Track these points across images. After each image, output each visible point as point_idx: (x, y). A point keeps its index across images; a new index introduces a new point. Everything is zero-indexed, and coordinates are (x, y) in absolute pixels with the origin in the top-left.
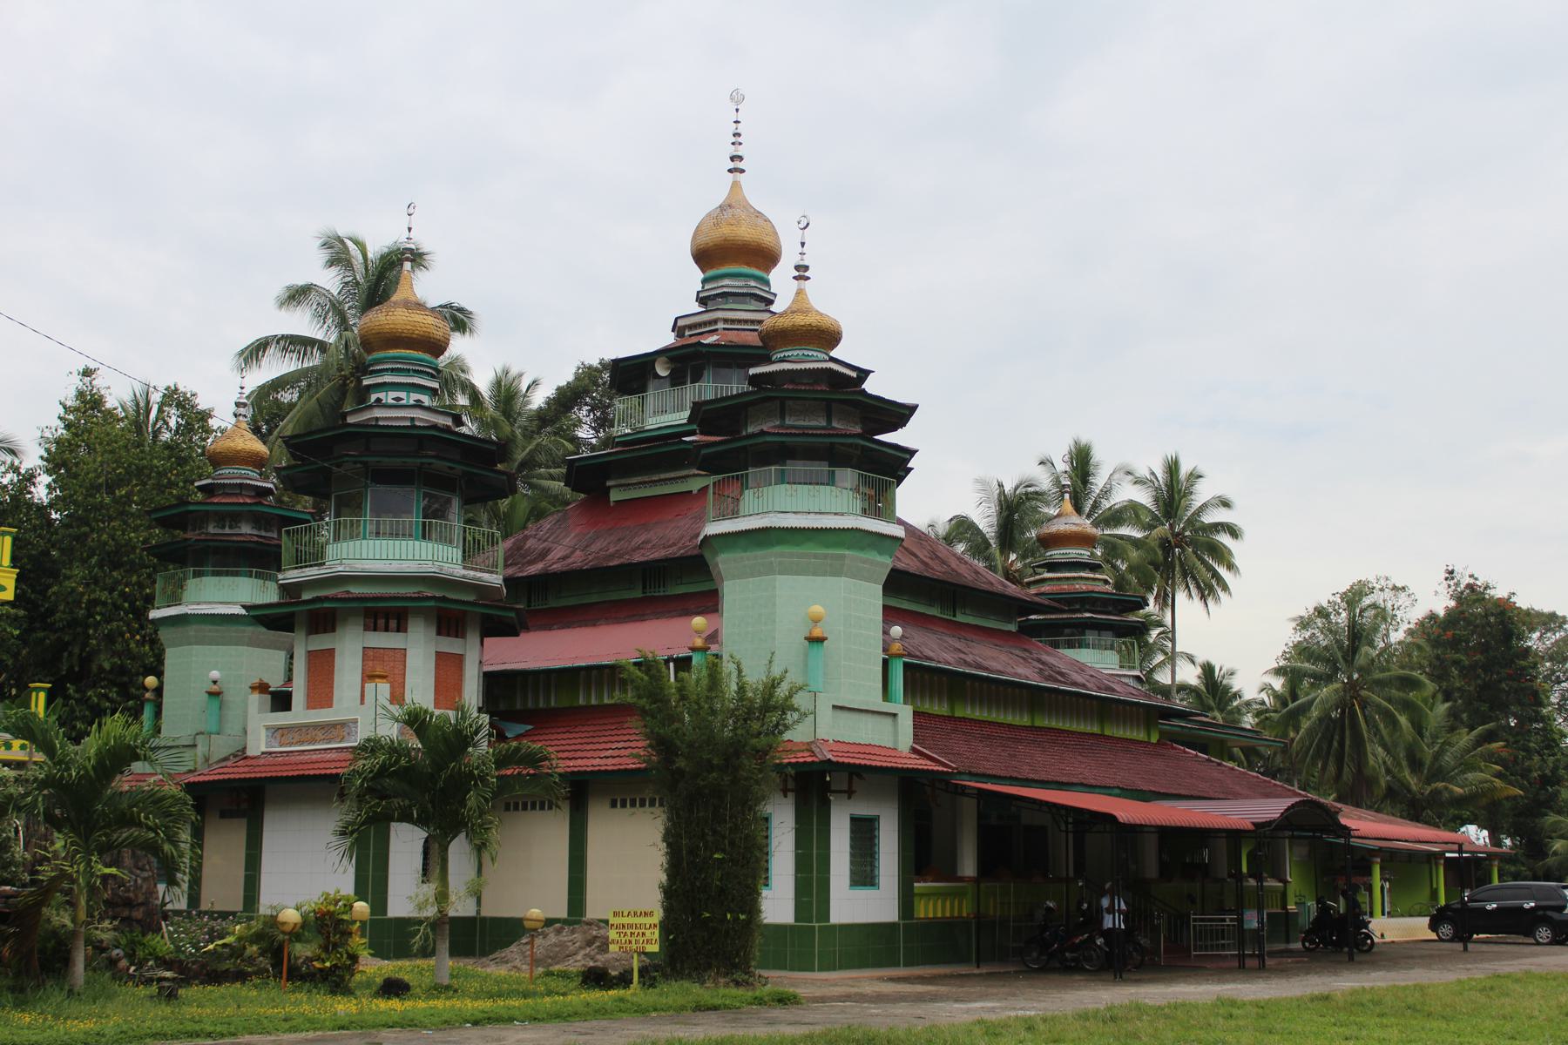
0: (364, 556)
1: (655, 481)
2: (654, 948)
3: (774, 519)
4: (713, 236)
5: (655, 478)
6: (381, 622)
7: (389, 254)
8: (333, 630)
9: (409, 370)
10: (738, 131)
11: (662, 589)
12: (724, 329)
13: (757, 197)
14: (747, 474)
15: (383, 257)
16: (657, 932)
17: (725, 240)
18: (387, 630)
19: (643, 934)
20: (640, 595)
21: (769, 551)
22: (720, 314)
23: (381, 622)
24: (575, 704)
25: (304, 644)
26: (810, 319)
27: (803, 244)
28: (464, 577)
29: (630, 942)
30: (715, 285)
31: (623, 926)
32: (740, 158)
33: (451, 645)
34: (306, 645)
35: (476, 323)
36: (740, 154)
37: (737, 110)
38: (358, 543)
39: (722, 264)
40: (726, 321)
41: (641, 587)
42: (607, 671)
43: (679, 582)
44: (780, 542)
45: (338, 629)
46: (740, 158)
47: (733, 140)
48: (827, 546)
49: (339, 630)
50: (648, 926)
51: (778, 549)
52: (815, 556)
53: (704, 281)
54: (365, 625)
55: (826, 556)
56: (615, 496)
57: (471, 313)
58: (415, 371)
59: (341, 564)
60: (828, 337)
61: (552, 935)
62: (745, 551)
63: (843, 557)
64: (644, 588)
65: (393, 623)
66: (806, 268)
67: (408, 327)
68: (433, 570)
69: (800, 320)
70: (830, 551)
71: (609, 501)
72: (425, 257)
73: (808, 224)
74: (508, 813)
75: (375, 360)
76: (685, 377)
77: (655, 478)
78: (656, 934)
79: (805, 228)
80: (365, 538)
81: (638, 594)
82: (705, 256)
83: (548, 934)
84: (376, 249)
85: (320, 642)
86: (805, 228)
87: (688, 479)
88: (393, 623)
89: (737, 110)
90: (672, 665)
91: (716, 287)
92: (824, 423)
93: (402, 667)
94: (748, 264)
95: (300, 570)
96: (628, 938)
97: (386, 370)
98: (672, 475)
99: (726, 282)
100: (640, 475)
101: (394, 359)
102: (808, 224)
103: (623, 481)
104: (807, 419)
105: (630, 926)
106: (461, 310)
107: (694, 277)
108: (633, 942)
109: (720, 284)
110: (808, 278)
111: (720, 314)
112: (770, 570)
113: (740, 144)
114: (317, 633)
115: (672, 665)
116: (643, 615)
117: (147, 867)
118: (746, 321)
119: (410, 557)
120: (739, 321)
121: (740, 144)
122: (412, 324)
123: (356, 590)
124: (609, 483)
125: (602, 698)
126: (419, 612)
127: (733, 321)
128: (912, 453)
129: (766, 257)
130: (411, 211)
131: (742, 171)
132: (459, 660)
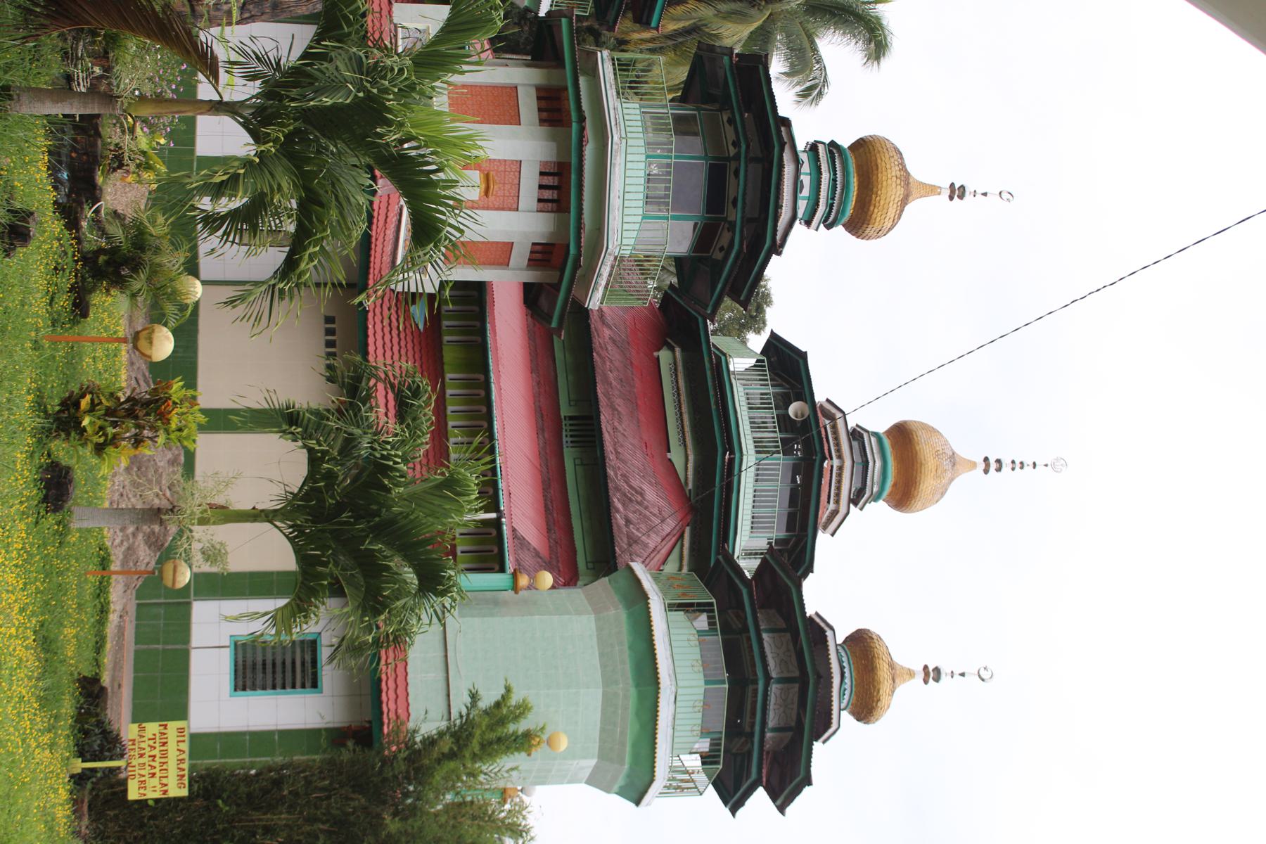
0: (629, 165)
1: (680, 407)
2: (133, 794)
3: (668, 691)
4: (926, 451)
5: (684, 409)
6: (549, 181)
7: (881, 25)
8: (542, 121)
9: (833, 199)
10: (1026, 467)
11: (569, 439)
12: (832, 467)
13: (966, 485)
14: (717, 635)
15: (878, 18)
16: (157, 795)
17: (921, 464)
18: (541, 187)
19: (153, 775)
20: (563, 415)
21: (631, 681)
22: (848, 463)
23: (549, 181)
24: (446, 367)
25: (526, 82)
26: (885, 687)
27: (963, 675)
28: (599, 274)
29: (141, 756)
30: (875, 451)
31: (164, 744)
32: (999, 470)
33: (520, 256)
34: (524, 85)
35: (807, 108)
36: (1004, 469)
37: (1046, 465)
38: (642, 150)
39: (896, 458)
40: (841, 468)
41: (574, 414)
42: (483, 393)
43: (578, 462)
44: (641, 697)
45: (545, 129)
46: (999, 470)
47: (1017, 462)
48: (634, 746)
49: (545, 129)
50: (164, 781)
51: (633, 692)
52: (623, 733)
53: (876, 434)
54: (547, 162)
55: (623, 744)
56: (664, 356)
57: (817, 104)
58: (832, 205)
59: (621, 138)
60: (865, 709)
61: (169, 455)
62: (630, 648)
63: (622, 762)
64: (571, 418)
65: (547, 194)
66: (937, 679)
67: (882, 202)
68: (610, 247)
69: (883, 672)
70: (628, 748)
71: (659, 350)
72: (876, 63)
73: (983, 680)
74: (323, 321)
75: (847, 159)
76: (786, 431)
77: (684, 409)
78: (152, 794)
79: (980, 676)
80: (648, 157)
81: (565, 411)
82: (902, 435)
83: (170, 449)
84: (886, 14)
85: (528, 105)
86: (980, 676)
87: (682, 448)
88: (547, 194)
89: (1046, 465)
90: (493, 515)
91: (871, 445)
92: (774, 675)
93: (497, 205)
94: (895, 485)
95: (613, 82)
96: (147, 752)
97: (835, 174)
98: (687, 429)
99: (878, 464)
100: (686, 387)
101: (846, 186)
102: (983, 680)
103: (680, 368)
104: (776, 707)
105: (164, 755)
106: (820, 94)
107: (877, 421)
108: (142, 761)
109: (876, 456)
110: (926, 682)
111: (848, 463)
112: (608, 681)
113: (1013, 469)
114: (539, 98)
115: (493, 515)
116: (543, 430)
117: (247, 15)
118: (839, 488)
119: (626, 204)
120: (839, 482)
121: (1013, 469)
122: (886, 206)
123: (589, 151)
124: (678, 350)
125: (449, 319)
126: (562, 227)
127: (840, 475)
128: (734, 811)
129: (903, 497)
130: (1005, 195)
131: (986, 471)
132: (504, 263)
